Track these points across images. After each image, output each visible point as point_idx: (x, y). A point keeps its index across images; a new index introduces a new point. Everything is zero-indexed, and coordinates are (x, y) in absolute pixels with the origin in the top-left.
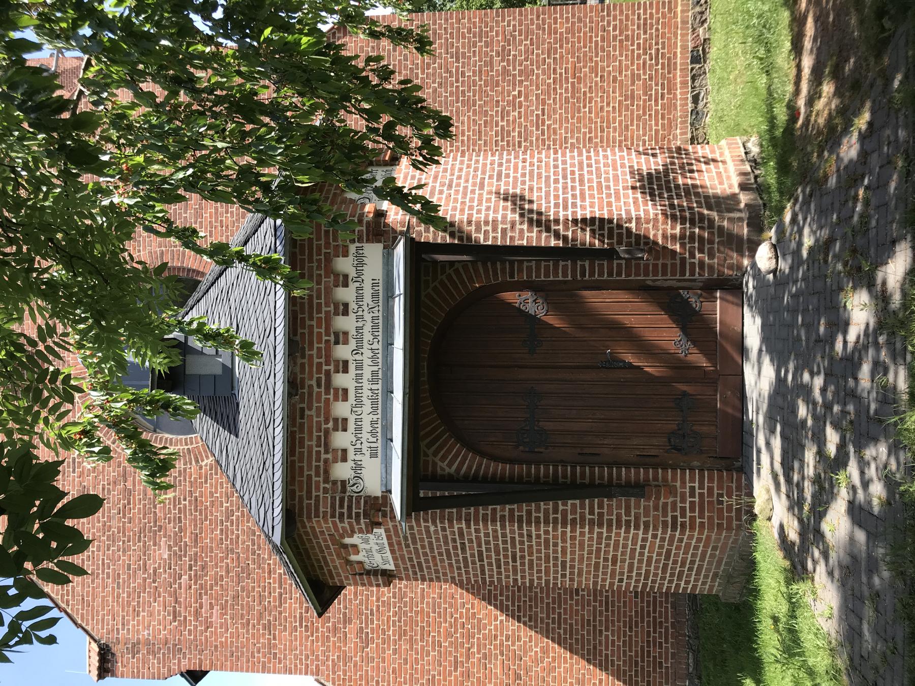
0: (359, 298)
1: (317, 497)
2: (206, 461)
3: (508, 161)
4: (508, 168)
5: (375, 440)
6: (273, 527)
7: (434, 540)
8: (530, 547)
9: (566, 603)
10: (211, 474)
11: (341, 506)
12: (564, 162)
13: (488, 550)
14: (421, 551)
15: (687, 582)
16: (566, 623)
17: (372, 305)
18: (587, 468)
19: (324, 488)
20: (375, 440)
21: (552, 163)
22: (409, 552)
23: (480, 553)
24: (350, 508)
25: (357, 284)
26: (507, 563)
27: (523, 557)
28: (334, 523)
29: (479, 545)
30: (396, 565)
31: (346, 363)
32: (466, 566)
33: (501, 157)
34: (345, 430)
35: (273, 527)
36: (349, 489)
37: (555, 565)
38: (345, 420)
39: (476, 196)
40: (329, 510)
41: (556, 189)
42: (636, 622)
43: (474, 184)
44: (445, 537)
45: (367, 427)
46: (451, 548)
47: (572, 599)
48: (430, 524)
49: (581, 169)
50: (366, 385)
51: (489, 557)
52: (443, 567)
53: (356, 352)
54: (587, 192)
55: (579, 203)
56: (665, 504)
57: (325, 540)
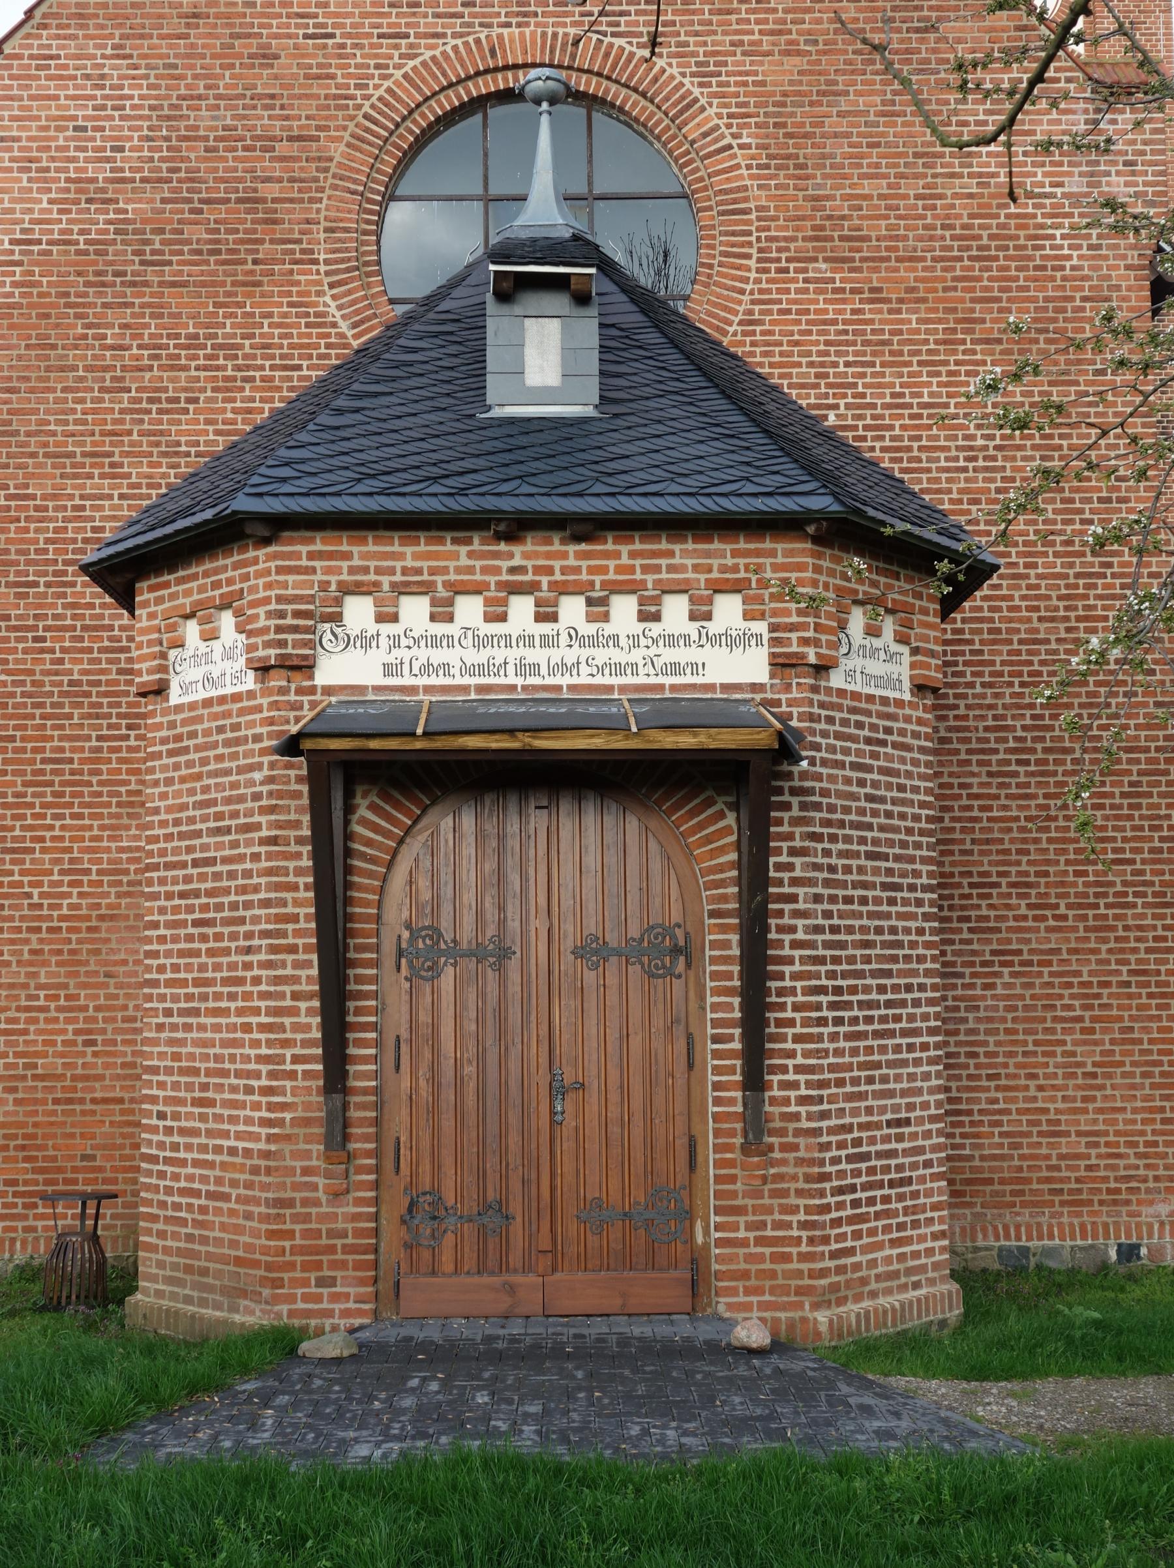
0: (671, 640)
1: (313, 570)
2: (333, 304)
3: (919, 903)
4: (906, 902)
5: (416, 671)
6: (260, 495)
7: (234, 778)
8: (227, 952)
9: (68, 1021)
10: (307, 315)
11: (297, 614)
12: (916, 1003)
13: (217, 876)
14: (211, 753)
15: (162, 1234)
16: (28, 1021)
17: (659, 662)
18: (372, 1051)
19: (328, 583)
20: (416, 671)
21: (915, 981)
22: (207, 733)
23: (211, 862)
24: (295, 629)
25: (695, 636)
26: (190, 909)
27: (204, 938)
28: (266, 601)
29: (226, 860)
30: (179, 708)
31: (554, 618)
32: (182, 836)
33: (926, 889)
34: (433, 618)
35: (260, 495)
36: (327, 626)
37: (189, 997)
38: (450, 618)
39: (855, 847)
40: (290, 592)
41: (867, 989)
42: (35, 1159)
43: (876, 842)
44: (241, 799)
45: (439, 656)
46: (219, 809)
47: (77, 1032)
48: (266, 772)
49: (905, 1033)
50: (513, 654)
51: (202, 877)
52: (178, 794)
53: (574, 635)
54: (862, 1044)
55: (841, 1029)
56: (315, 1188)
57: (230, 581)
